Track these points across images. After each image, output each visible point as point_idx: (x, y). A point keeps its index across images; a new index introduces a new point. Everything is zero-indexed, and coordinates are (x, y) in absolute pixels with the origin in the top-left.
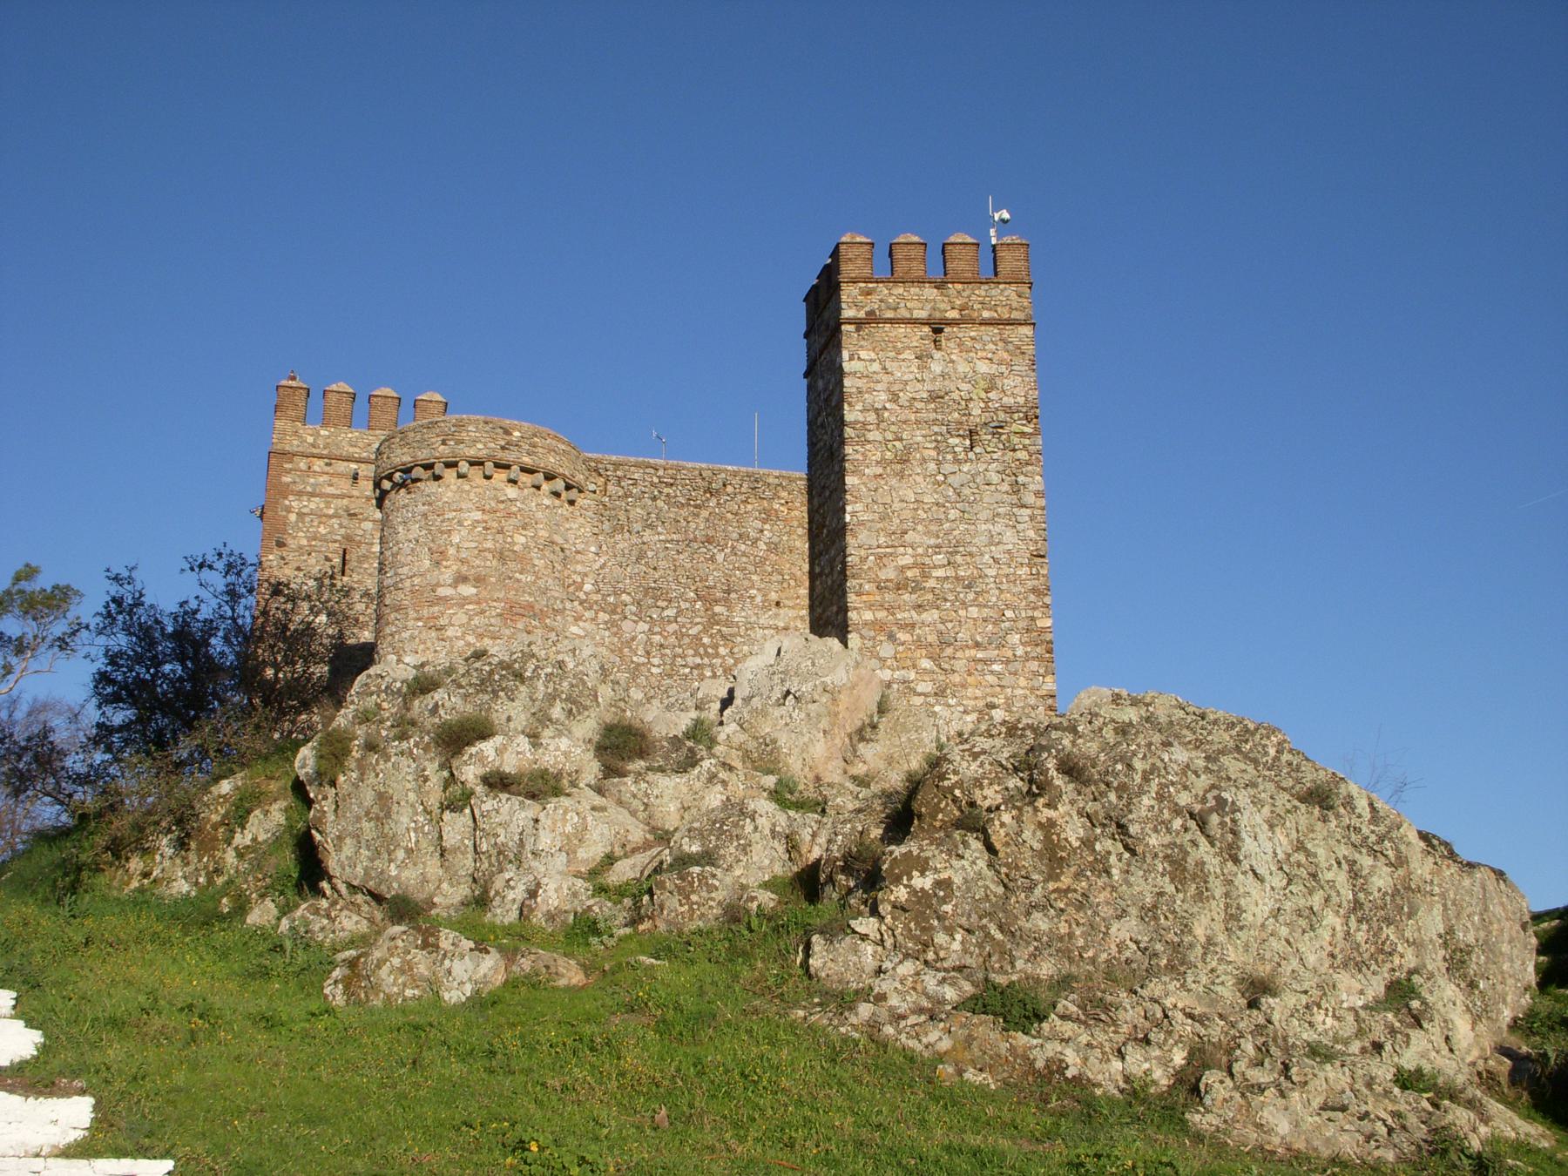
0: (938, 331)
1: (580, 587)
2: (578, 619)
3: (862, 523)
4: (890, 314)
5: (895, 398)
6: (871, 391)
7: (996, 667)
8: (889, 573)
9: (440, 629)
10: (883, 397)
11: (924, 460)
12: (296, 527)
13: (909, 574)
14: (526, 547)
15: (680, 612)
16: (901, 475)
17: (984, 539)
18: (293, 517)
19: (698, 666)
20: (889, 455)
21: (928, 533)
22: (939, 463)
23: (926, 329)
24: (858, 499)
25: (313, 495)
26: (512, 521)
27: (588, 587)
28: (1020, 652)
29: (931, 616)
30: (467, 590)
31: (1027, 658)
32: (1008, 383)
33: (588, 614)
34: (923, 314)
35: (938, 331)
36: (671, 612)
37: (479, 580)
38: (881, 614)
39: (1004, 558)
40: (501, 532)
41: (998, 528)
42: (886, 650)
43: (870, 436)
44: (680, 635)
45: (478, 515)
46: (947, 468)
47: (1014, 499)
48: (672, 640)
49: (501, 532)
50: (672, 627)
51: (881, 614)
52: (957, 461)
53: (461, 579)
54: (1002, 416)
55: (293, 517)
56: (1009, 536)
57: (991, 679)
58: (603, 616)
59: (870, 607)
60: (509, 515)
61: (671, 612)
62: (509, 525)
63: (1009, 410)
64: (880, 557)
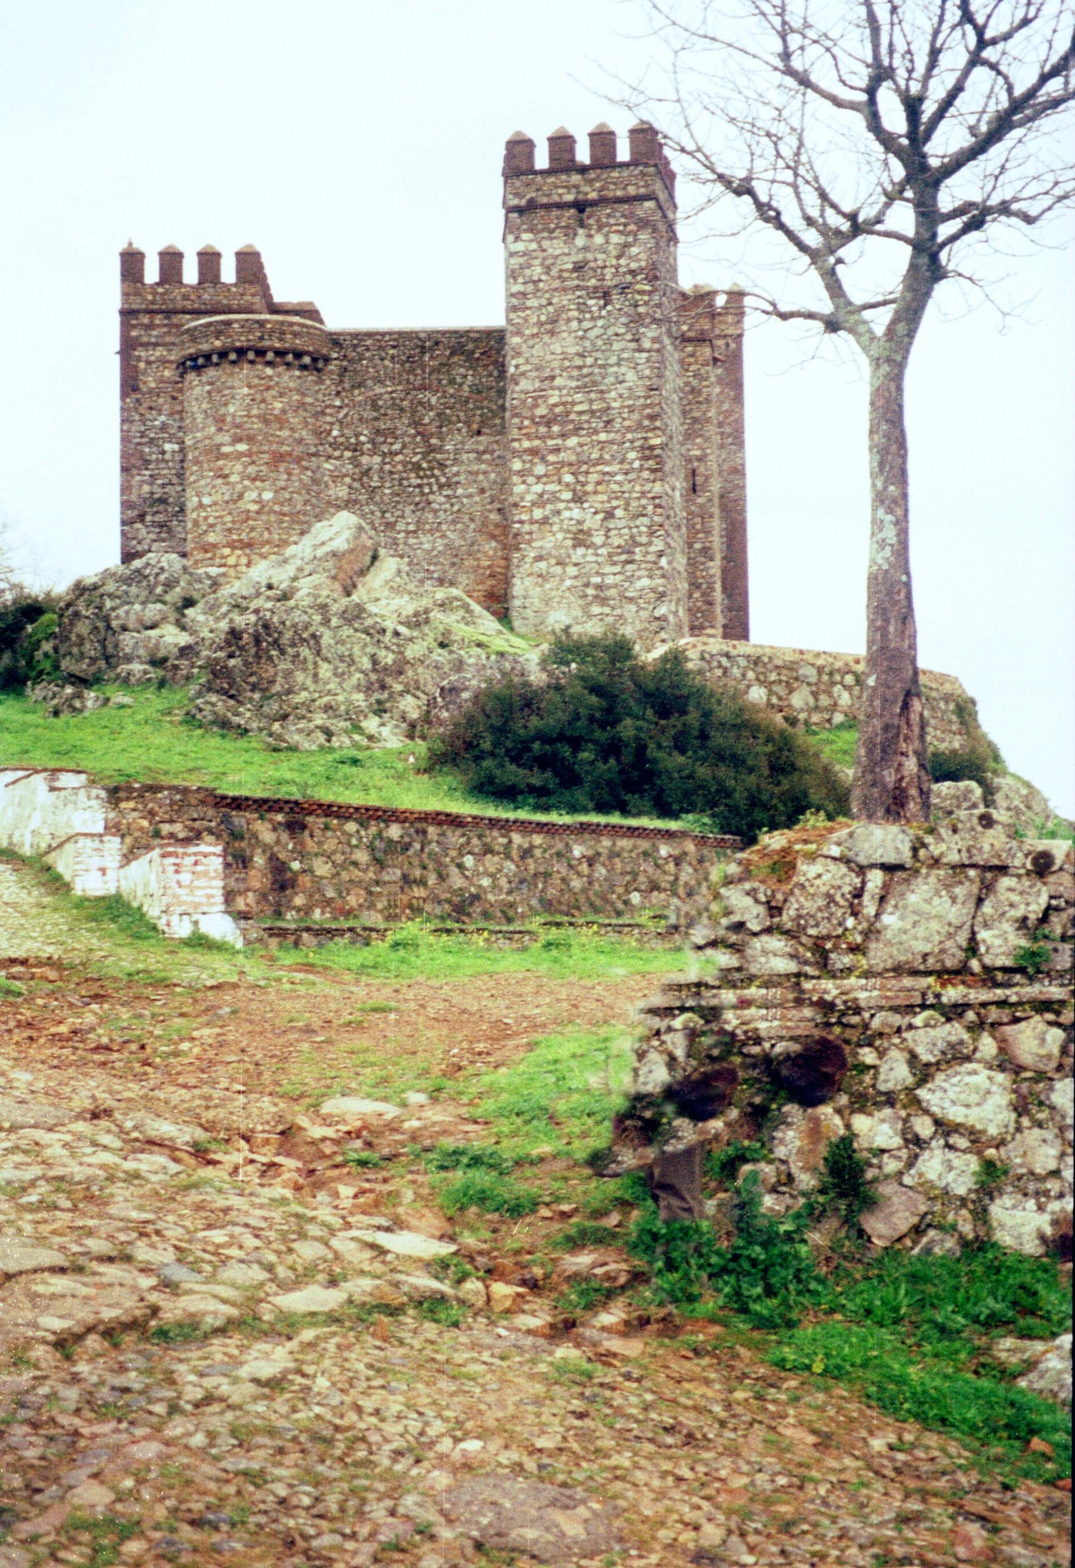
0: (581, 211)
1: (329, 432)
2: (329, 457)
3: (523, 374)
4: (545, 200)
5: (548, 269)
6: (529, 266)
7: (619, 478)
8: (541, 411)
9: (226, 476)
10: (539, 270)
11: (569, 320)
12: (145, 373)
13: (557, 410)
14: (284, 411)
15: (404, 447)
16: (552, 333)
17: (612, 379)
18: (142, 365)
19: (420, 486)
20: (543, 318)
21: (571, 377)
22: (580, 321)
23: (572, 211)
24: (518, 354)
25: (156, 345)
26: (273, 392)
27: (335, 433)
28: (637, 464)
29: (572, 441)
30: (242, 447)
31: (641, 469)
32: (634, 250)
33: (337, 453)
34: (570, 198)
35: (581, 211)
36: (397, 447)
37: (250, 439)
38: (537, 443)
39: (626, 394)
40: (263, 401)
41: (623, 369)
42: (540, 469)
43: (529, 303)
44: (404, 463)
45: (246, 390)
46: (586, 325)
47: (633, 345)
48: (400, 467)
49: (263, 401)
50: (399, 458)
51: (537, 443)
52: (593, 319)
53: (237, 440)
54: (629, 278)
55: (142, 365)
56: (631, 376)
57: (615, 487)
58: (348, 454)
59: (528, 436)
60: (268, 388)
61: (397, 447)
62: (268, 395)
63: (633, 272)
64: (535, 399)
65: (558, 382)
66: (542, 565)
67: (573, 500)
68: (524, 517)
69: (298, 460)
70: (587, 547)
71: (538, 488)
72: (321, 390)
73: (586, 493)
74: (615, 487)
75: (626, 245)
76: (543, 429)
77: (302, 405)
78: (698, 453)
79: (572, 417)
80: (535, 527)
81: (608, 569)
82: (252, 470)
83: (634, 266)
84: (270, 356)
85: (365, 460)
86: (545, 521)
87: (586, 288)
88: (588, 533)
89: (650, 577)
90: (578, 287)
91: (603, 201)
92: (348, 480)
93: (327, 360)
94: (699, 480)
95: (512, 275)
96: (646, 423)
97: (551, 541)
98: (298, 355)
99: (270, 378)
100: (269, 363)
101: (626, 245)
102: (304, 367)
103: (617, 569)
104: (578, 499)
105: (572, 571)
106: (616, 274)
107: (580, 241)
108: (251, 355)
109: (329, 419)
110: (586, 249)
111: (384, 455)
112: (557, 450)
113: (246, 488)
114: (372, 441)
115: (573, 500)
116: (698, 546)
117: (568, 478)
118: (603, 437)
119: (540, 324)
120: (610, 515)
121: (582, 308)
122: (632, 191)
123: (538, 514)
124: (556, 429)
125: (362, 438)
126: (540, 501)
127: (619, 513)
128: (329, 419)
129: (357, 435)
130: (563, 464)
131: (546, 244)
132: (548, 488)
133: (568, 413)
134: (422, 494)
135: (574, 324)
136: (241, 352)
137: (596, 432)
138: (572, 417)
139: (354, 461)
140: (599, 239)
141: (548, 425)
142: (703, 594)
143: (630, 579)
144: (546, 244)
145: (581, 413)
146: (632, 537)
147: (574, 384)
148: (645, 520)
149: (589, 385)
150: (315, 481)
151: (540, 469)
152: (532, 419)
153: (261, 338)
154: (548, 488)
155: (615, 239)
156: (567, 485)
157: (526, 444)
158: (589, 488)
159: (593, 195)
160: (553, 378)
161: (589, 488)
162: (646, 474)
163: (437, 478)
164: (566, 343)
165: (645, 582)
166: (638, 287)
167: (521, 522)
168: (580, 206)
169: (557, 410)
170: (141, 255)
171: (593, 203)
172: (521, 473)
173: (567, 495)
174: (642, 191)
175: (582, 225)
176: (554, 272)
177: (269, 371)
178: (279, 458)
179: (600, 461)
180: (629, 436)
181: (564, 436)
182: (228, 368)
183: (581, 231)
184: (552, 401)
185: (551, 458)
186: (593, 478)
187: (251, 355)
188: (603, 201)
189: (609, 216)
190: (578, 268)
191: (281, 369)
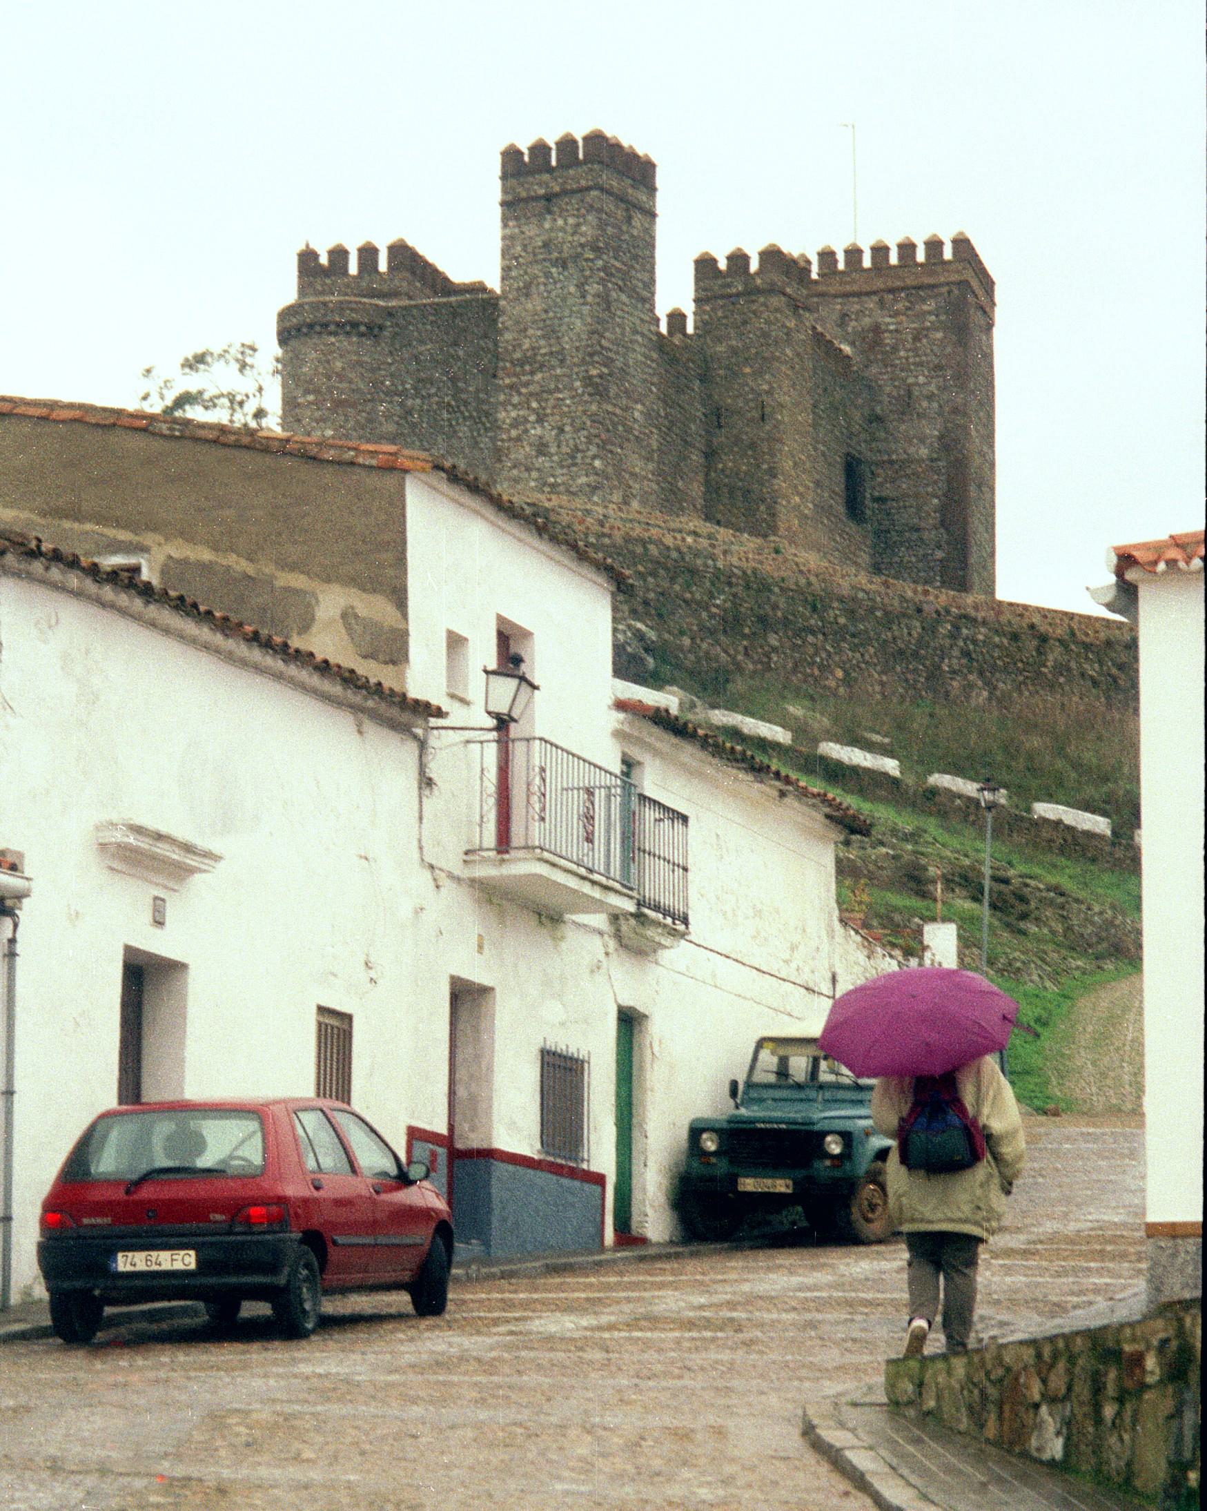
2: (383, 401)
5: (525, 247)
8: (518, 355)
14: (343, 369)
21: (538, 329)
22: (545, 285)
28: (580, 391)
29: (538, 377)
30: (311, 398)
31: (583, 394)
34: (542, 192)
37: (317, 391)
47: (581, 301)
48: (435, 407)
53: (307, 392)
54: (579, 250)
56: (578, 323)
57: (565, 409)
59: (508, 376)
63: (582, 246)
65: (530, 332)
66: (515, 472)
67: (537, 421)
68: (504, 437)
69: (354, 405)
70: (545, 455)
71: (513, 414)
72: (367, 351)
73: (546, 415)
74: (565, 409)
75: (578, 225)
76: (518, 369)
77: (360, 363)
78: (765, 387)
79: (539, 358)
80: (511, 444)
81: (559, 471)
82: (318, 414)
83: (583, 240)
84: (332, 328)
85: (409, 402)
86: (518, 439)
87: (550, 260)
88: (546, 445)
89: (587, 475)
90: (544, 260)
91: (565, 192)
92: (396, 419)
93: (381, 328)
94: (768, 410)
95: (505, 253)
96: (587, 358)
97: (524, 451)
98: (354, 325)
99: (333, 344)
100: (331, 334)
101: (578, 225)
102: (362, 335)
103: (565, 471)
104: (540, 420)
105: (534, 474)
106: (573, 247)
107: (547, 225)
108: (318, 328)
109: (383, 373)
110: (552, 229)
111: (423, 397)
112: (526, 384)
113: (313, 429)
114: (415, 388)
115: (537, 421)
116: (765, 466)
117: (534, 405)
118: (559, 371)
119: (519, 289)
120: (561, 430)
121: (548, 275)
122: (583, 183)
123: (514, 433)
124: (527, 368)
125: (408, 386)
126: (515, 424)
127: (567, 428)
128: (383, 373)
129: (403, 383)
130: (531, 394)
131: (525, 229)
132: (521, 413)
133: (535, 355)
134: (451, 425)
135: (542, 288)
136: (311, 326)
137: (553, 368)
138: (539, 358)
139: (402, 404)
140: (560, 222)
141: (522, 366)
142: (768, 508)
143: (573, 478)
144: (525, 229)
145: (545, 354)
146: (576, 446)
147: (539, 333)
148: (585, 433)
149: (551, 333)
150: (370, 421)
151: (516, 400)
152: (512, 362)
153: (325, 315)
154: (521, 413)
155: (571, 221)
156: (534, 410)
157: (507, 381)
158: (549, 411)
159: (557, 189)
160: (526, 330)
161: (549, 411)
162: (586, 398)
163: (462, 413)
164: (535, 304)
165: (583, 480)
166: (587, 256)
167: (503, 440)
168: (549, 198)
169: (529, 354)
170: (887, 249)
171: (557, 195)
172: (504, 404)
173: (532, 418)
174: (590, 183)
175: (550, 212)
176: (530, 249)
177: (333, 339)
178: (338, 404)
179: (558, 390)
180: (576, 370)
181: (532, 373)
182: (303, 339)
183: (548, 217)
184: (525, 347)
185: (524, 390)
186: (551, 402)
187: (318, 328)
188: (565, 192)
189: (567, 204)
190: (546, 245)
191: (341, 337)
